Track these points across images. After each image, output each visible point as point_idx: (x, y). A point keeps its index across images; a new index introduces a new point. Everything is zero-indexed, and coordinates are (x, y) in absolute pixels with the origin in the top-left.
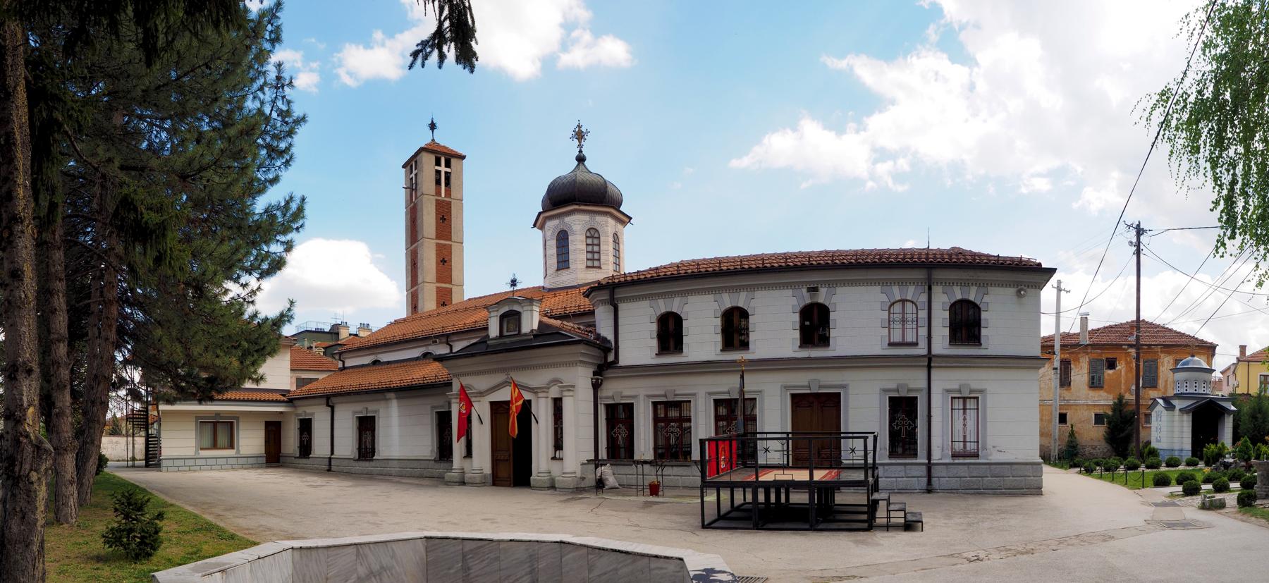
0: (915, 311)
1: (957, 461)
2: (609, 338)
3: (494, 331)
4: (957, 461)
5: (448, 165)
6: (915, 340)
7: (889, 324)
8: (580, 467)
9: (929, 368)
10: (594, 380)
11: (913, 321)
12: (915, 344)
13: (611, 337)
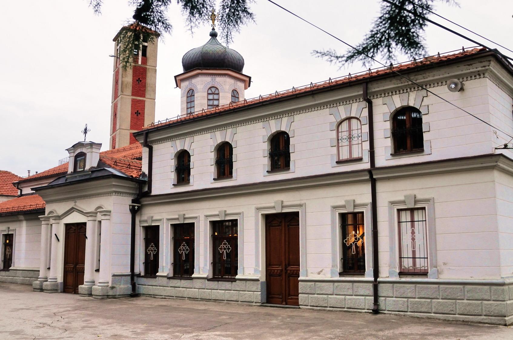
0: (359, 127)
1: (403, 279)
2: (146, 174)
4: (403, 279)
6: (360, 156)
7: (338, 143)
8: (111, 278)
9: (374, 183)
10: (131, 207)
11: (358, 137)
12: (360, 160)
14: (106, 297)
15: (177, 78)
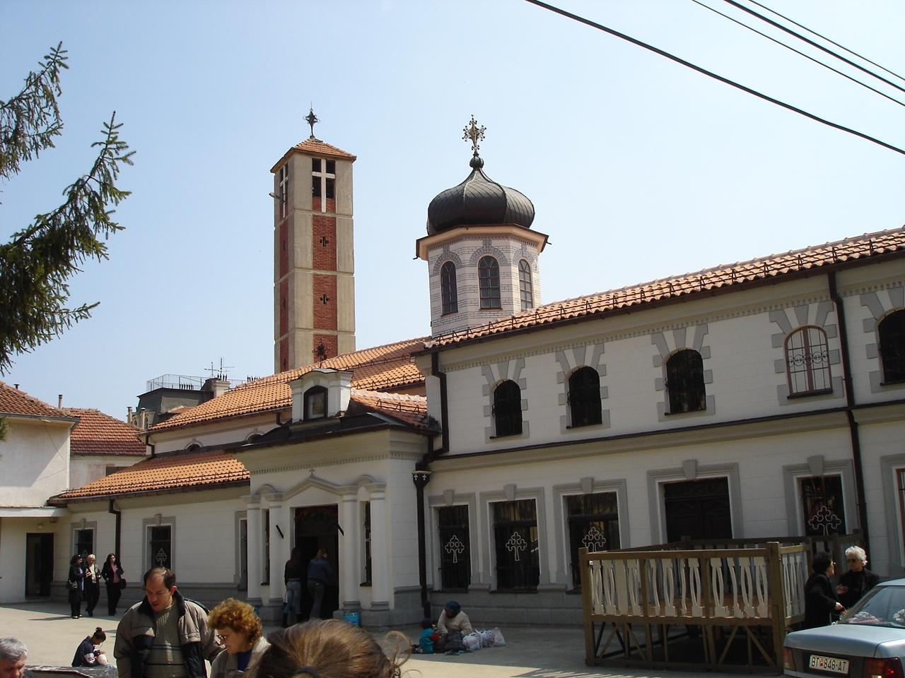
3: (297, 414)
5: (331, 168)
6: (828, 386)
7: (788, 367)
10: (416, 476)
12: (828, 392)
13: (438, 416)
14: (387, 628)
15: (421, 244)
